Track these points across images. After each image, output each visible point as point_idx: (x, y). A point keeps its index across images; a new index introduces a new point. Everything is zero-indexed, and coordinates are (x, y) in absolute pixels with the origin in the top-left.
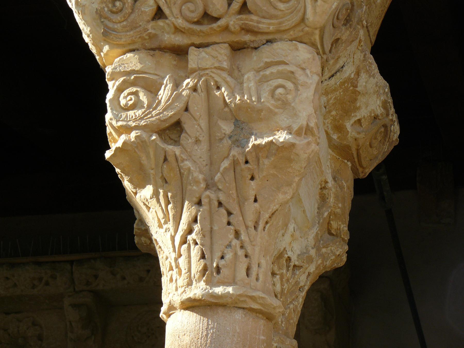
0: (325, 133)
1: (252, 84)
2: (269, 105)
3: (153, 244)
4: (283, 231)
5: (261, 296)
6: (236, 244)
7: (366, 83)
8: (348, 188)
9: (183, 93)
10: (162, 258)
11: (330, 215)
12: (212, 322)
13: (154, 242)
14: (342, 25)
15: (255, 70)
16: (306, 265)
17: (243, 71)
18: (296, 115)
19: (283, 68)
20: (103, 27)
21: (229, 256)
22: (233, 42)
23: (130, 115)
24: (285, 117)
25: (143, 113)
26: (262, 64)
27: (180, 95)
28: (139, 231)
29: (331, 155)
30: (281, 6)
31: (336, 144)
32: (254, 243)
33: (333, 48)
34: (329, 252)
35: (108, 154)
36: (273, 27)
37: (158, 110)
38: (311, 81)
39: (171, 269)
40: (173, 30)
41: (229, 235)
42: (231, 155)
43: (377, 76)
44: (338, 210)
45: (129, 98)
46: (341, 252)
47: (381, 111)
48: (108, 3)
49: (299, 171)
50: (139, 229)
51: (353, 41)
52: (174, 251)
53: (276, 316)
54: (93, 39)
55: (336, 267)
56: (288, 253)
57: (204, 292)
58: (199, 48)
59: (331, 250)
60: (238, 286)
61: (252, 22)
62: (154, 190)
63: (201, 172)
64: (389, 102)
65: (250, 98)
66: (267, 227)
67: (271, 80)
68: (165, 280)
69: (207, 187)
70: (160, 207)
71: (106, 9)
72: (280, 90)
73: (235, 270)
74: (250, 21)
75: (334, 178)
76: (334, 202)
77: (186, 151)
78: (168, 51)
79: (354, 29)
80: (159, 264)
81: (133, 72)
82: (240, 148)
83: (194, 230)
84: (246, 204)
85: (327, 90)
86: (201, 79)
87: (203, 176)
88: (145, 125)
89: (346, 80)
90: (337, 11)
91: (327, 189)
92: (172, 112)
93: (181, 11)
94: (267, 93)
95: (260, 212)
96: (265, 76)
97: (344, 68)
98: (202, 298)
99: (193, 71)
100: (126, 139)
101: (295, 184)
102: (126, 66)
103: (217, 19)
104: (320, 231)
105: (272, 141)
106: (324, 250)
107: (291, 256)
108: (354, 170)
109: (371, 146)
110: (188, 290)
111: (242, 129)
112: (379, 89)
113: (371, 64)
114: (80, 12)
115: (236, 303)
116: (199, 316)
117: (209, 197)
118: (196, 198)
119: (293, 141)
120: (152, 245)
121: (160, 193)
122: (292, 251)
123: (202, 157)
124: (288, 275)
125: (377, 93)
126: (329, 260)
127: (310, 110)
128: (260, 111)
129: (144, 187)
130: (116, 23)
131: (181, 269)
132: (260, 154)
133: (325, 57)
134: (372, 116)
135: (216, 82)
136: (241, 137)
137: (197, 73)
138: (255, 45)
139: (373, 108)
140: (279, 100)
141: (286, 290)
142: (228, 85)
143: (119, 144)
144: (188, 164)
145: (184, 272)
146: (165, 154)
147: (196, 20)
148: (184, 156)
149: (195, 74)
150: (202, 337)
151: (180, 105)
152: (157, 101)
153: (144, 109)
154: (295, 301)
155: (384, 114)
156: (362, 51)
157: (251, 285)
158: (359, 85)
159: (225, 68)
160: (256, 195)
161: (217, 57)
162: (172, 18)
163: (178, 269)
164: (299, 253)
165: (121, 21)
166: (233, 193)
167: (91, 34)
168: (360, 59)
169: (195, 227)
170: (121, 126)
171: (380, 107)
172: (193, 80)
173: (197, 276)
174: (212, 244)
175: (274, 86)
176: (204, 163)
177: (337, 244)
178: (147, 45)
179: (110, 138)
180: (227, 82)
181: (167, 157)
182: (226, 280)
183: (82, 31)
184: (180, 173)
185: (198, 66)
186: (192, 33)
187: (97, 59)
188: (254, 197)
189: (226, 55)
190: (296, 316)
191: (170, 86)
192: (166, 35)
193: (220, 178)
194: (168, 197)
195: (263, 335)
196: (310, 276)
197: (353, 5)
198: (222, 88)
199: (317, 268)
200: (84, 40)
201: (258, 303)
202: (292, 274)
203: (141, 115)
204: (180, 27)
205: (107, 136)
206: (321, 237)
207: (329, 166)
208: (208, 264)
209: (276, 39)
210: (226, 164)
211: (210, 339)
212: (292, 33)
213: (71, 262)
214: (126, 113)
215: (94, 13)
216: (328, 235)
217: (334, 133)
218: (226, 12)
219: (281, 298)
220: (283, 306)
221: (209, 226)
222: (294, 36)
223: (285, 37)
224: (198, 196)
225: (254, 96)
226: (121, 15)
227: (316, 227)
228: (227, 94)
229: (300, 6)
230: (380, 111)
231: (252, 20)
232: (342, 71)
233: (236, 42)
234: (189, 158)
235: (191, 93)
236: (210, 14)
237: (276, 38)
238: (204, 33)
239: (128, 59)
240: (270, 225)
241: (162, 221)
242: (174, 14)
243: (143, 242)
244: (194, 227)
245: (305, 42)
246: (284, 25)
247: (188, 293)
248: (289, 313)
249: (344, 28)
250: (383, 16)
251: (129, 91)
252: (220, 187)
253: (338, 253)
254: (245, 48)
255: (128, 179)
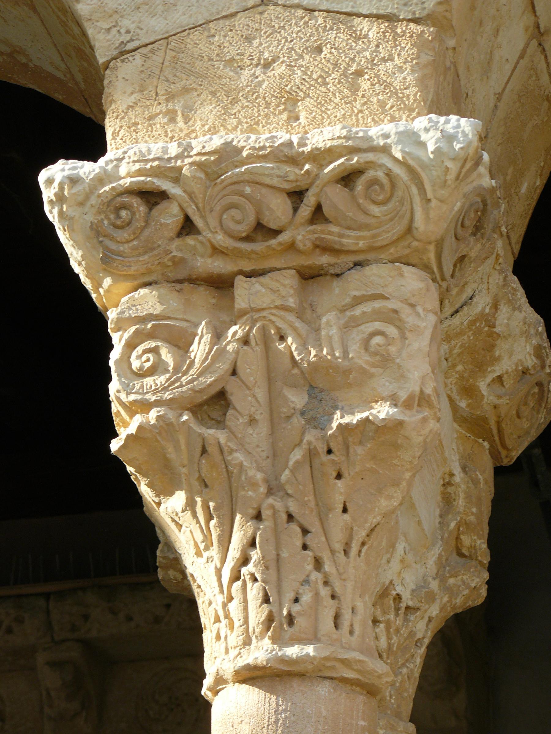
0: (447, 399)
1: (334, 331)
2: (361, 362)
3: (188, 581)
4: (388, 556)
5: (358, 658)
6: (316, 579)
7: (508, 319)
8: (486, 482)
9: (228, 348)
10: (203, 602)
11: (458, 526)
12: (283, 701)
13: (190, 578)
14: (470, 235)
15: (337, 309)
16: (424, 606)
17: (319, 311)
18: (402, 376)
19: (381, 305)
20: (101, 250)
21: (306, 598)
22: (303, 266)
23: (147, 384)
24: (387, 381)
25: (168, 380)
26: (348, 300)
27: (222, 351)
28: (165, 561)
29: (457, 431)
30: (376, 210)
31: (465, 415)
32: (344, 577)
33: (457, 271)
34: (460, 583)
35: (115, 445)
36: (363, 242)
37: (191, 376)
38: (425, 324)
39: (217, 620)
40: (209, 251)
41: (306, 564)
42: (305, 441)
43: (524, 309)
44: (472, 518)
45: (144, 358)
46: (477, 583)
47: (533, 361)
48: (109, 214)
49: (411, 463)
50: (164, 558)
51: (487, 258)
52: (222, 592)
53: (382, 688)
54: (88, 270)
55: (472, 606)
56: (397, 588)
57: (270, 655)
58: (250, 277)
59: (462, 580)
60: (322, 645)
61: (330, 235)
62: (187, 499)
63: (259, 469)
64: (545, 347)
65: (332, 352)
66: (364, 550)
67: (363, 323)
68: (207, 637)
69: (270, 492)
70: (198, 525)
71: (106, 222)
72: (378, 340)
73: (316, 619)
74: (329, 234)
75: (464, 469)
76: (465, 506)
77: (235, 436)
78: (202, 283)
79: (489, 240)
80: (198, 612)
81: (149, 317)
82: (319, 430)
83: (251, 558)
84: (330, 516)
85: (448, 333)
86: (255, 326)
87: (263, 474)
88: (171, 399)
89: (478, 318)
90: (460, 215)
91: (453, 485)
92: (212, 377)
93: (221, 222)
94: (358, 344)
95: (352, 529)
96: (353, 318)
97: (475, 300)
98: (267, 664)
99: (243, 313)
100: (143, 421)
101: (404, 484)
102: (139, 309)
103: (276, 233)
104: (445, 552)
105: (367, 419)
106: (452, 581)
107: (401, 593)
108: (494, 454)
109: (519, 417)
110: (245, 651)
111: (321, 400)
112: (529, 328)
113: (514, 290)
114: (66, 228)
115: (320, 670)
116: (264, 693)
117: (272, 507)
118: (254, 509)
119: (400, 417)
120: (186, 582)
121: (196, 502)
122: (403, 584)
123: (260, 445)
124: (398, 622)
125: (526, 334)
126: (461, 596)
127: (426, 368)
128: (347, 372)
129: (171, 494)
130: (122, 243)
131: (232, 620)
132: (350, 439)
133: (444, 285)
134: (519, 370)
135: (278, 329)
136: (319, 414)
137: (248, 316)
138: (336, 271)
139: (520, 358)
140: (376, 354)
141: (395, 645)
142: (226, 186)
143: (132, 429)
144: (239, 457)
145: (237, 624)
146: (204, 443)
147: (244, 234)
148: (232, 446)
149: (245, 318)
150: (269, 725)
151: (224, 366)
152: (188, 362)
153: (169, 375)
154: (410, 662)
155: (538, 366)
156: (501, 272)
157: (341, 641)
158: (497, 323)
159: (291, 307)
160: (345, 502)
161: (279, 290)
162: (208, 234)
163: (229, 620)
164: (414, 587)
165: (129, 240)
166: (309, 500)
167: (83, 260)
168: (498, 283)
169: (252, 553)
170: (135, 401)
171: (530, 355)
172: (243, 327)
173: (258, 630)
174: (279, 580)
175: (368, 333)
176: (264, 455)
177: (472, 570)
178: (170, 274)
179: (118, 419)
180: (295, 329)
181: (207, 448)
182: (303, 636)
183: (69, 256)
184: (227, 471)
185: (250, 306)
186: (238, 254)
187: (95, 300)
188: (342, 506)
189: (292, 287)
190: (411, 686)
191: (207, 337)
192: (199, 258)
193: (289, 478)
194: (209, 508)
195: (363, 719)
196: (431, 623)
197: (485, 204)
198: (287, 338)
199: (442, 609)
200: (72, 270)
201: (353, 669)
202: (404, 621)
203: (165, 384)
204: (221, 246)
205: (112, 418)
206: (447, 559)
207: (456, 450)
208: (274, 611)
209: (368, 260)
210: (297, 455)
211: (281, 729)
212: (392, 250)
213: (47, 596)
214: (141, 381)
215: (88, 228)
216: (457, 557)
217: (461, 399)
218: (291, 223)
219: (388, 658)
220: (392, 674)
221: (274, 552)
222: (396, 256)
223: (382, 256)
224: (255, 506)
225: (338, 349)
226: (130, 230)
227: (438, 545)
228: (296, 348)
229: (404, 209)
230: (531, 362)
231: (330, 233)
232: (471, 304)
233: (306, 267)
234: (240, 446)
235: (240, 347)
236: (266, 225)
237: (369, 259)
238: (257, 254)
239: (142, 297)
240: (369, 548)
241: (202, 546)
242: (211, 227)
243: (172, 577)
244: (251, 553)
245: (413, 263)
246: (380, 238)
247: (244, 657)
248: (402, 681)
249: (472, 239)
250: (531, 212)
251: (144, 346)
252: (290, 492)
253: (473, 585)
254: (320, 275)
255: (147, 482)
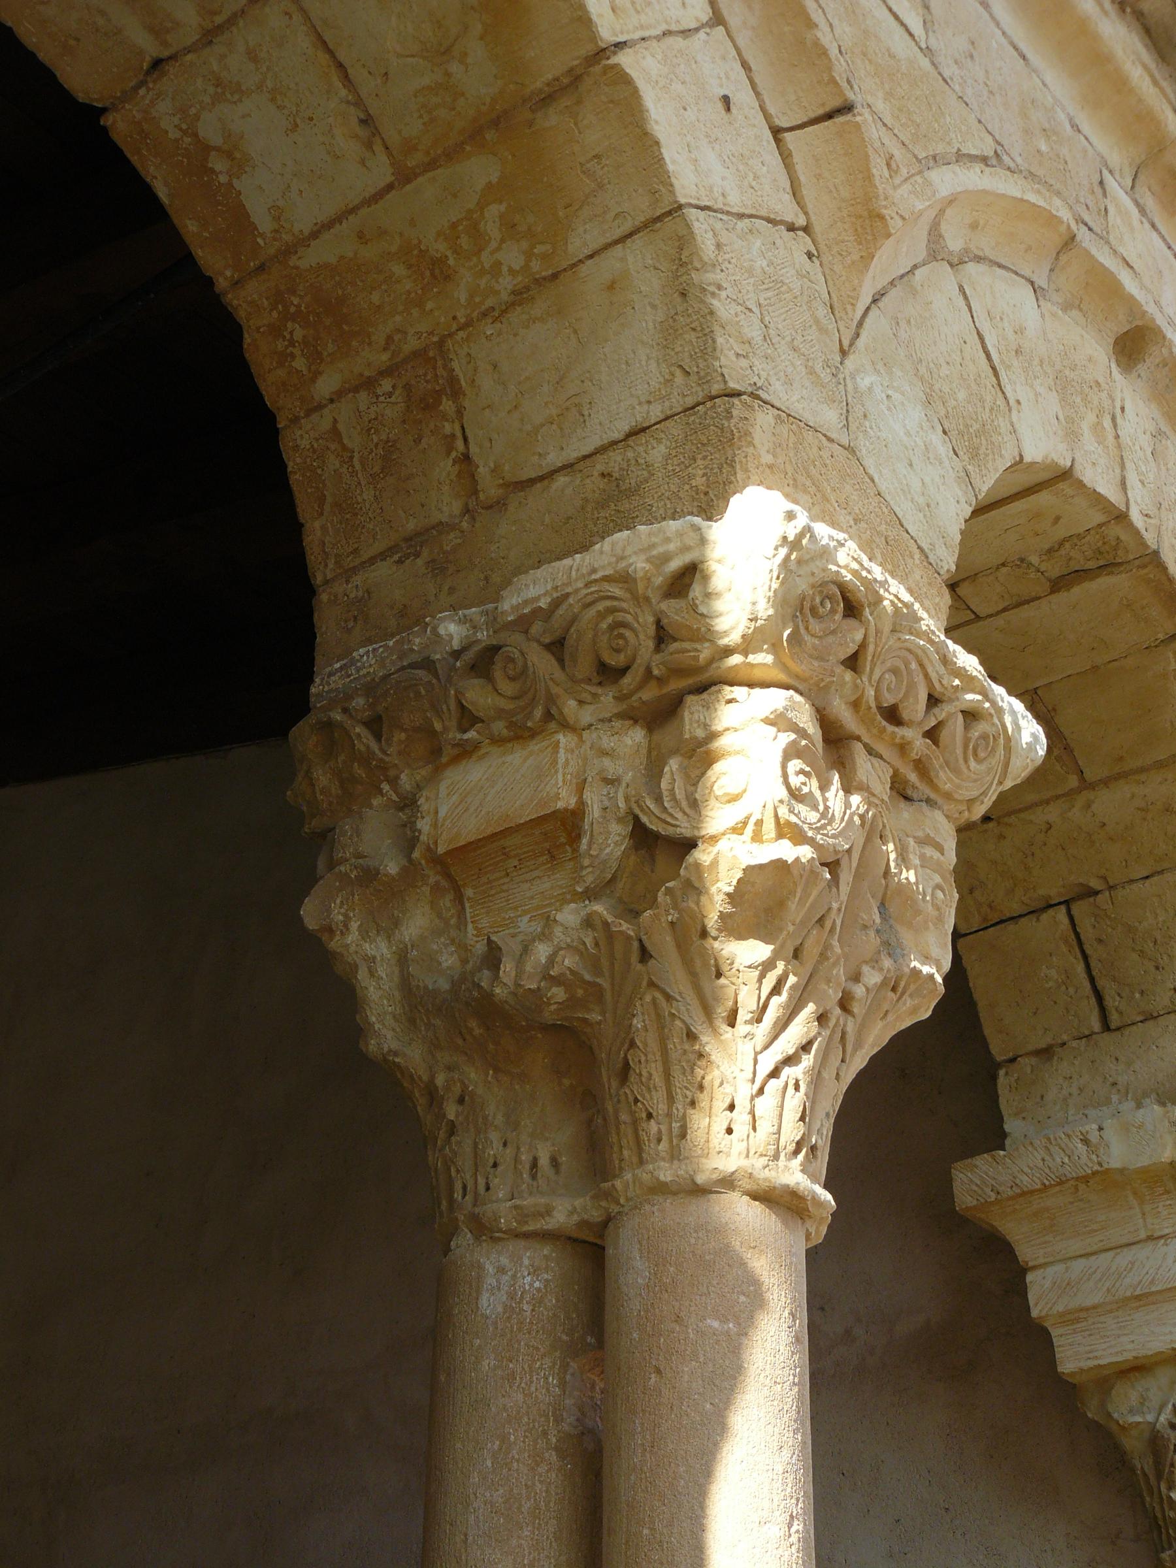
40: (853, 698)
88: (822, 845)
114: (781, 576)
